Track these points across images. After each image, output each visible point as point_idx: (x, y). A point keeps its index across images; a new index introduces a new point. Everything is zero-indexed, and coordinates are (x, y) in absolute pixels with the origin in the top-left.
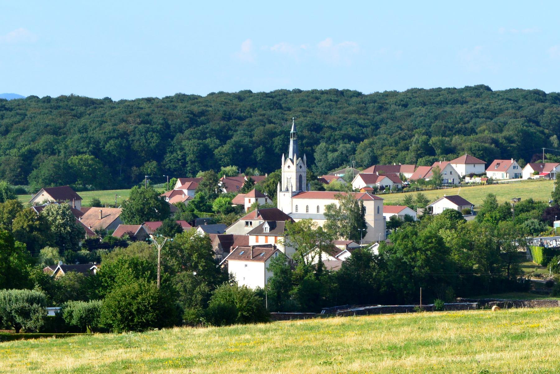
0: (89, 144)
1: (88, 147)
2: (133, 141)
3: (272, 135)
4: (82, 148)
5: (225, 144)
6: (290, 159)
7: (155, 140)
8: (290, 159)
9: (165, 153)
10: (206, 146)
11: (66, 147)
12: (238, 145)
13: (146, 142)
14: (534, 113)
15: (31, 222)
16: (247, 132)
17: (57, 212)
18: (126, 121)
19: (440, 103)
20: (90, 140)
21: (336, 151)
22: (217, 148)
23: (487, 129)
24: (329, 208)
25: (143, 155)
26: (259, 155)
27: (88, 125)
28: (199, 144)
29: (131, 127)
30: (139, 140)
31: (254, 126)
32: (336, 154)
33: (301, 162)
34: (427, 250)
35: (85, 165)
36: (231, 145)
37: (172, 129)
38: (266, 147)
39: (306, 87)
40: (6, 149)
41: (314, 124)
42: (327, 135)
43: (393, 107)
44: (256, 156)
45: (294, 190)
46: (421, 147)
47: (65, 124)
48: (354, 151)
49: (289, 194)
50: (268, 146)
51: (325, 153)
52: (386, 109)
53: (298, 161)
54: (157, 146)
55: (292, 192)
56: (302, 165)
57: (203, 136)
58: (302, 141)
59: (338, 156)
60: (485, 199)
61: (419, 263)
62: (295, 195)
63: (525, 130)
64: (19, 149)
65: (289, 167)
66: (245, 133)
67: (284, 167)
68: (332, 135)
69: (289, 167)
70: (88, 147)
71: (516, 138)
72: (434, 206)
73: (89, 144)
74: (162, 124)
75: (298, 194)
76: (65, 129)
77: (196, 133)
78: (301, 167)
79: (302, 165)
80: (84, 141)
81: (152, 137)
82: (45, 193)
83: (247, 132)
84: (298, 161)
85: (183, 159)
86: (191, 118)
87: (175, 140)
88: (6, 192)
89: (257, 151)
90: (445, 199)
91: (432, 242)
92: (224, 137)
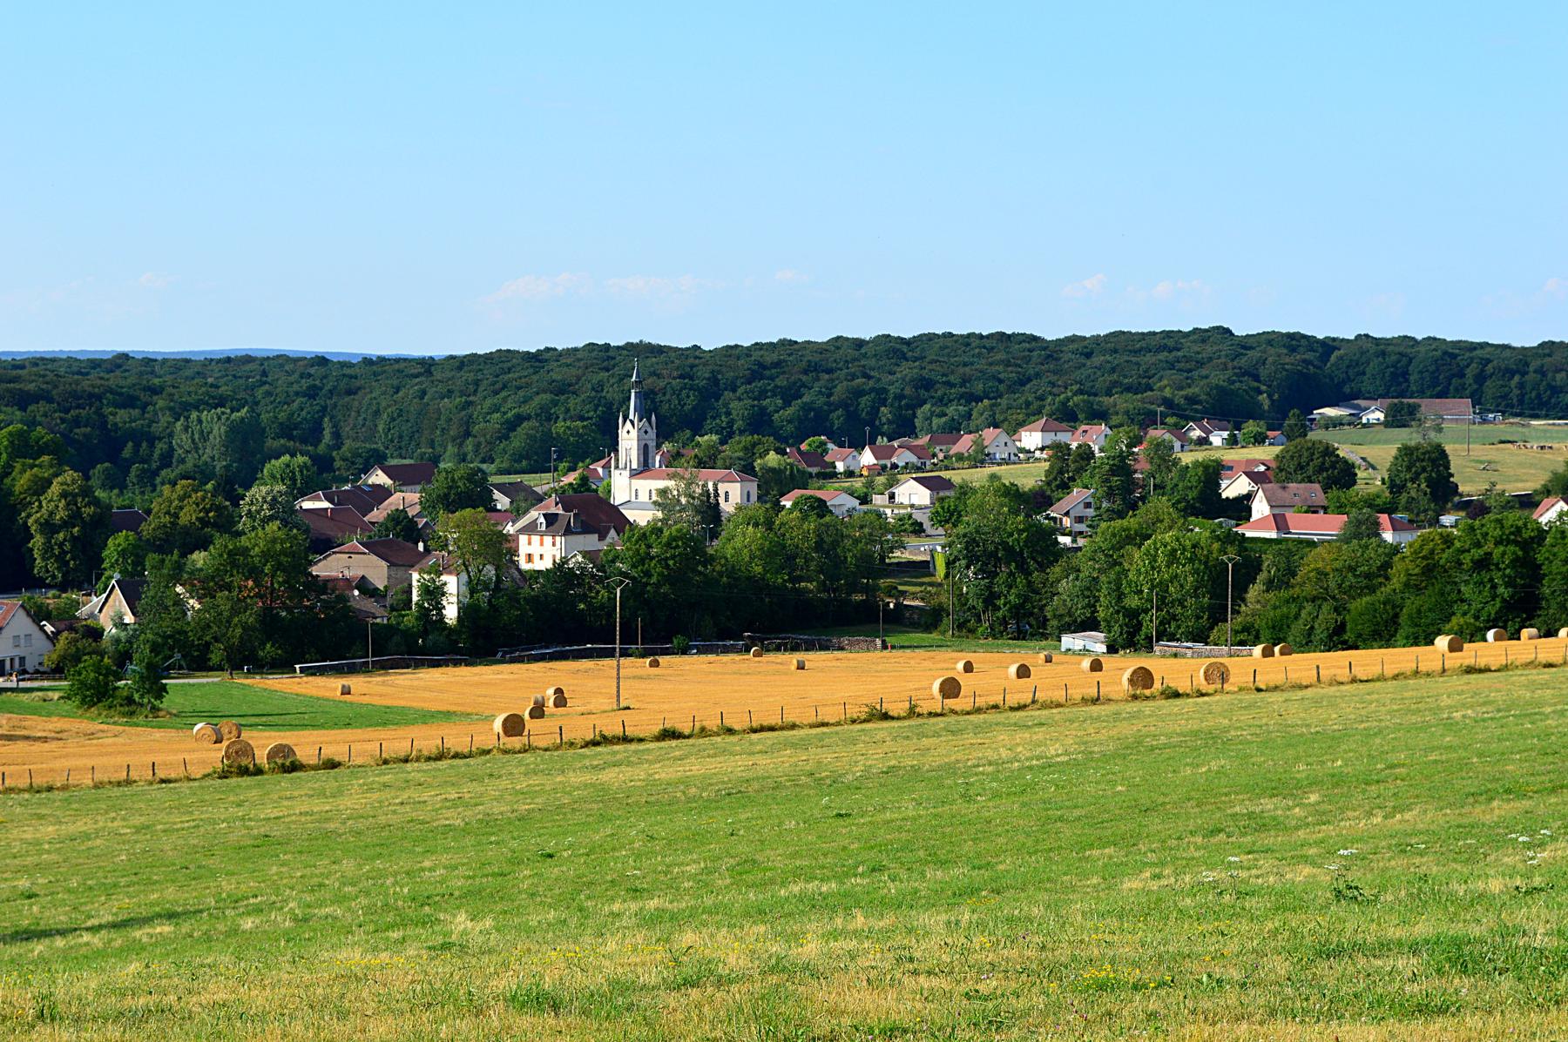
0: (597, 406)
1: (595, 411)
2: (661, 402)
3: (859, 393)
4: (588, 412)
5: (790, 406)
6: (631, 421)
7: (691, 401)
8: (631, 421)
9: (706, 419)
10: (763, 410)
11: (568, 410)
12: (807, 408)
13: (679, 404)
14: (1254, 362)
15: (202, 514)
16: (823, 390)
17: (263, 498)
18: (659, 376)
19: (1137, 352)
20: (599, 401)
21: (946, 415)
22: (778, 412)
23: (1168, 385)
24: (663, 492)
25: (673, 421)
26: (836, 422)
27: (605, 380)
28: (753, 406)
29: (662, 384)
30: (669, 401)
31: (837, 382)
32: (944, 419)
33: (647, 424)
34: (667, 559)
35: (572, 435)
36: (797, 408)
37: (722, 386)
38: (848, 411)
39: (960, 330)
40: (488, 413)
41: (923, 379)
42: (939, 393)
43: (1066, 357)
44: (832, 424)
45: (635, 466)
46: (1057, 410)
47: (579, 379)
48: (969, 416)
49: (627, 473)
50: (852, 409)
51: (929, 419)
52: (1057, 359)
53: (641, 424)
54: (694, 408)
55: (631, 470)
56: (649, 430)
57: (762, 395)
58: (900, 401)
59: (945, 423)
60: (1543, 482)
61: (654, 580)
62: (634, 474)
63: (1222, 387)
64: (505, 413)
65: (628, 432)
66: (820, 391)
67: (622, 433)
68: (945, 394)
69: (628, 432)
70: (595, 411)
71: (1203, 397)
72: (896, 491)
73: (597, 406)
74: (709, 379)
75: (641, 472)
76: (577, 387)
77: (753, 392)
78: (646, 432)
79: (649, 430)
80: (590, 403)
81: (688, 397)
82: (380, 472)
83: (823, 390)
84: (641, 424)
85: (729, 427)
86: (753, 371)
87: (721, 401)
88: (301, 471)
89: (834, 415)
90: (912, 480)
91: (677, 546)
92: (790, 395)
